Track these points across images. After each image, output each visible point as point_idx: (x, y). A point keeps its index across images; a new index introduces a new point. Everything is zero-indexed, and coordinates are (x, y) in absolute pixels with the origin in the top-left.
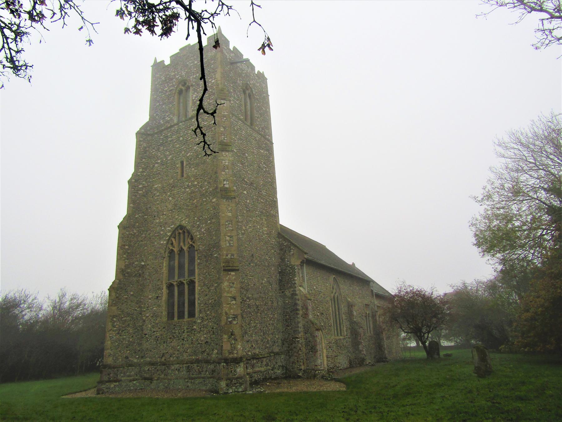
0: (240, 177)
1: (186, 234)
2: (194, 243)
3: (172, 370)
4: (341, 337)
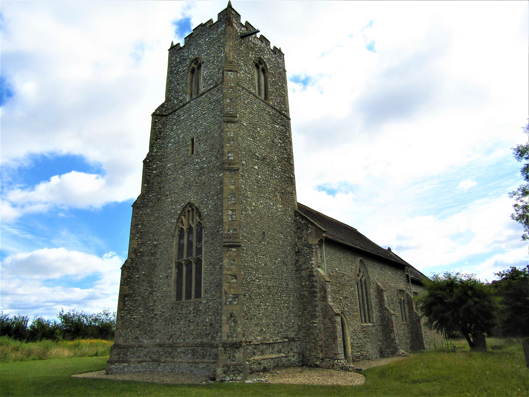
0: (251, 151)
1: (195, 212)
2: (201, 220)
3: (178, 352)
4: (370, 324)
